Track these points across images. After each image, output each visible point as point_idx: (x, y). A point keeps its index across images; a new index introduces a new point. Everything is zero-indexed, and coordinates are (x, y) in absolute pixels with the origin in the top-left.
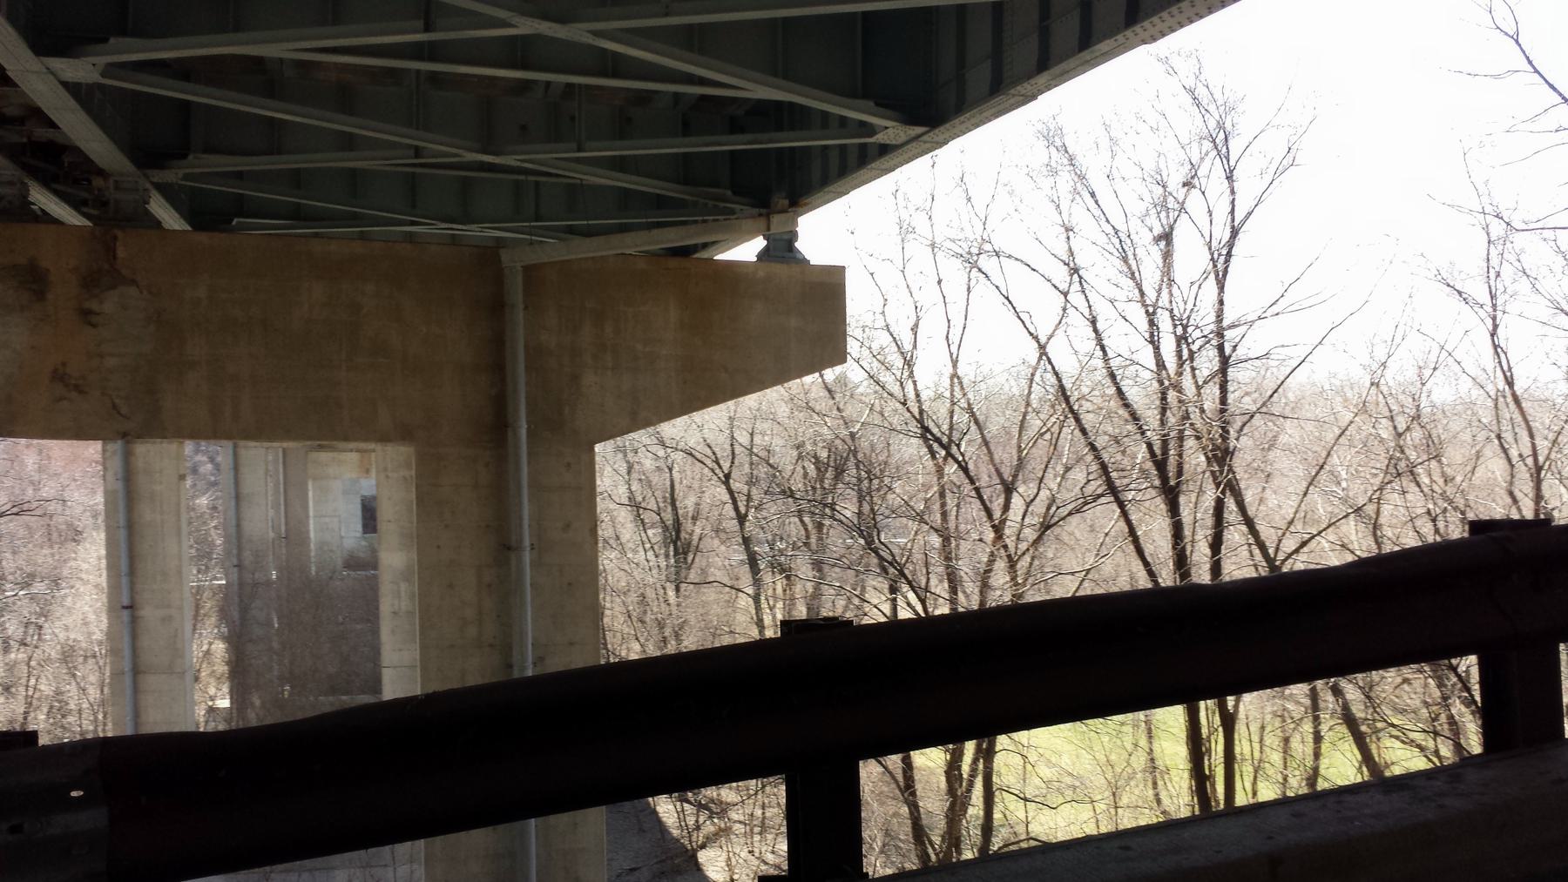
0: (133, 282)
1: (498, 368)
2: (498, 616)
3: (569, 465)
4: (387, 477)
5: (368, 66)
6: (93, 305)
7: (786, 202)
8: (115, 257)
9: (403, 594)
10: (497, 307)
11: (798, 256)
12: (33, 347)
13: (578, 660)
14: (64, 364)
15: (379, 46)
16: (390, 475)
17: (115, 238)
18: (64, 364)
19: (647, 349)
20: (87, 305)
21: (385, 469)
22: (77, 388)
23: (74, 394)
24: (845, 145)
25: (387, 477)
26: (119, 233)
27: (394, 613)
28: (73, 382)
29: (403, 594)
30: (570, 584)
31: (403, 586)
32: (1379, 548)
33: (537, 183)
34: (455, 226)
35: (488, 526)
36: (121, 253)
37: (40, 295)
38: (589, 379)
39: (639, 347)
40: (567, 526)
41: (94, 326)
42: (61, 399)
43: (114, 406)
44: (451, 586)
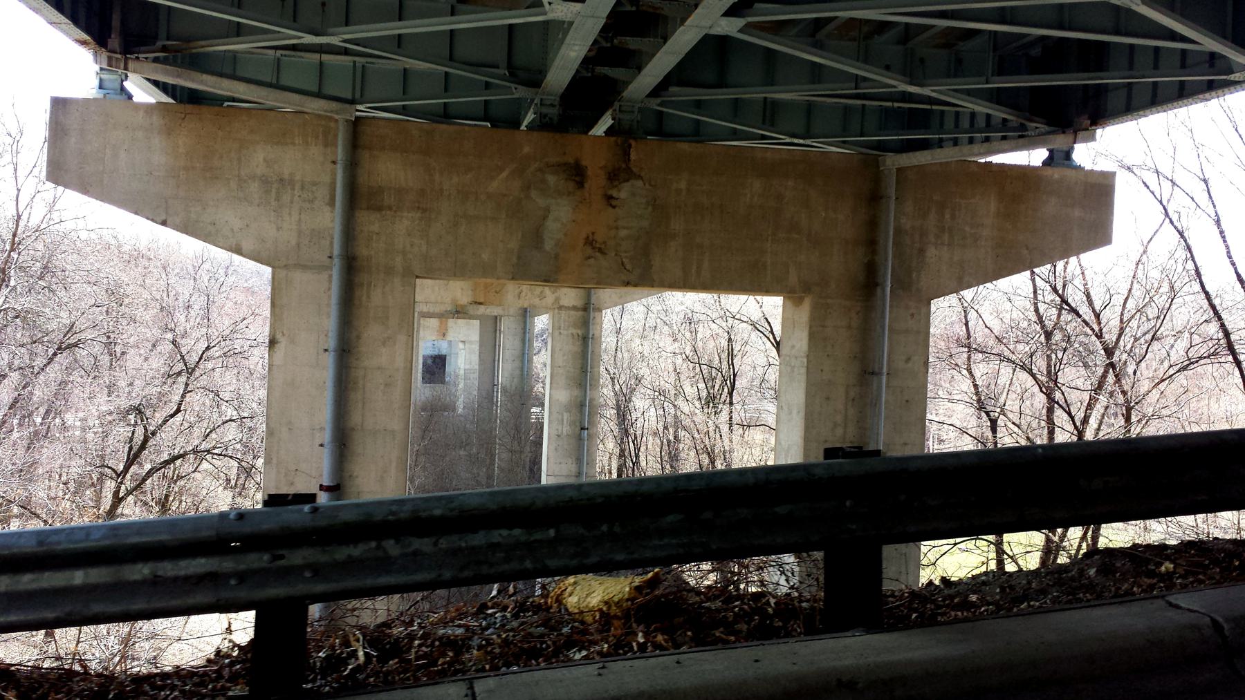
0: (639, 177)
1: (871, 243)
2: (858, 422)
3: (912, 315)
4: (560, 333)
5: (758, 22)
6: (614, 193)
7: (1089, 122)
8: (629, 160)
9: (565, 421)
10: (875, 198)
11: (1074, 164)
12: (574, 221)
13: (909, 451)
14: (593, 234)
15: (930, 11)
16: (562, 331)
17: (630, 146)
18: (593, 234)
19: (972, 231)
20: (610, 192)
21: (560, 328)
22: (600, 250)
23: (598, 254)
24: (1157, 82)
25: (560, 333)
26: (633, 143)
27: (558, 436)
28: (598, 246)
29: (565, 421)
30: (907, 401)
31: (566, 416)
32: (1051, 433)
33: (942, 112)
34: (796, 141)
35: (855, 357)
36: (633, 156)
37: (581, 185)
38: (932, 252)
39: (967, 229)
40: (908, 360)
41: (614, 207)
42: (589, 258)
43: (623, 264)
44: (828, 398)
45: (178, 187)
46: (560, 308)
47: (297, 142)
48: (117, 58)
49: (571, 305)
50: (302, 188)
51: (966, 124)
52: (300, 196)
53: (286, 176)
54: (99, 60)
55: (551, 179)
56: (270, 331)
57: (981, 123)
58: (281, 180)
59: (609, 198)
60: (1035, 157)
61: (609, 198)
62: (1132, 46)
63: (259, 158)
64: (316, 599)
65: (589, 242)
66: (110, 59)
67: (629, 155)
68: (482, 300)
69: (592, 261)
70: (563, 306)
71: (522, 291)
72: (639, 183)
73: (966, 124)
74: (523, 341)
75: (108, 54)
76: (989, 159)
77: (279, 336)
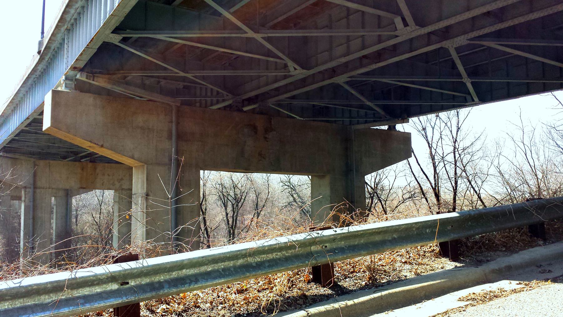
6: (267, 136)
17: (271, 119)
18: (261, 151)
22: (264, 158)
36: (272, 123)
41: (267, 141)
42: (260, 160)
45: (108, 130)
46: (123, 189)
47: (154, 113)
48: (90, 76)
49: (127, 188)
50: (157, 132)
51: (209, 94)
52: (156, 135)
53: (150, 127)
54: (82, 76)
55: (246, 130)
56: (146, 191)
57: (215, 93)
58: (149, 129)
59: (266, 138)
60: (385, 127)
61: (266, 138)
62: (431, 91)
63: (140, 120)
64: (142, 300)
65: (260, 154)
66: (87, 76)
67: (271, 122)
68: (84, 187)
69: (261, 162)
70: (124, 189)
71: (104, 182)
72: (275, 133)
73: (209, 94)
74: (67, 209)
75: (86, 73)
76: (378, 127)
77: (150, 193)
